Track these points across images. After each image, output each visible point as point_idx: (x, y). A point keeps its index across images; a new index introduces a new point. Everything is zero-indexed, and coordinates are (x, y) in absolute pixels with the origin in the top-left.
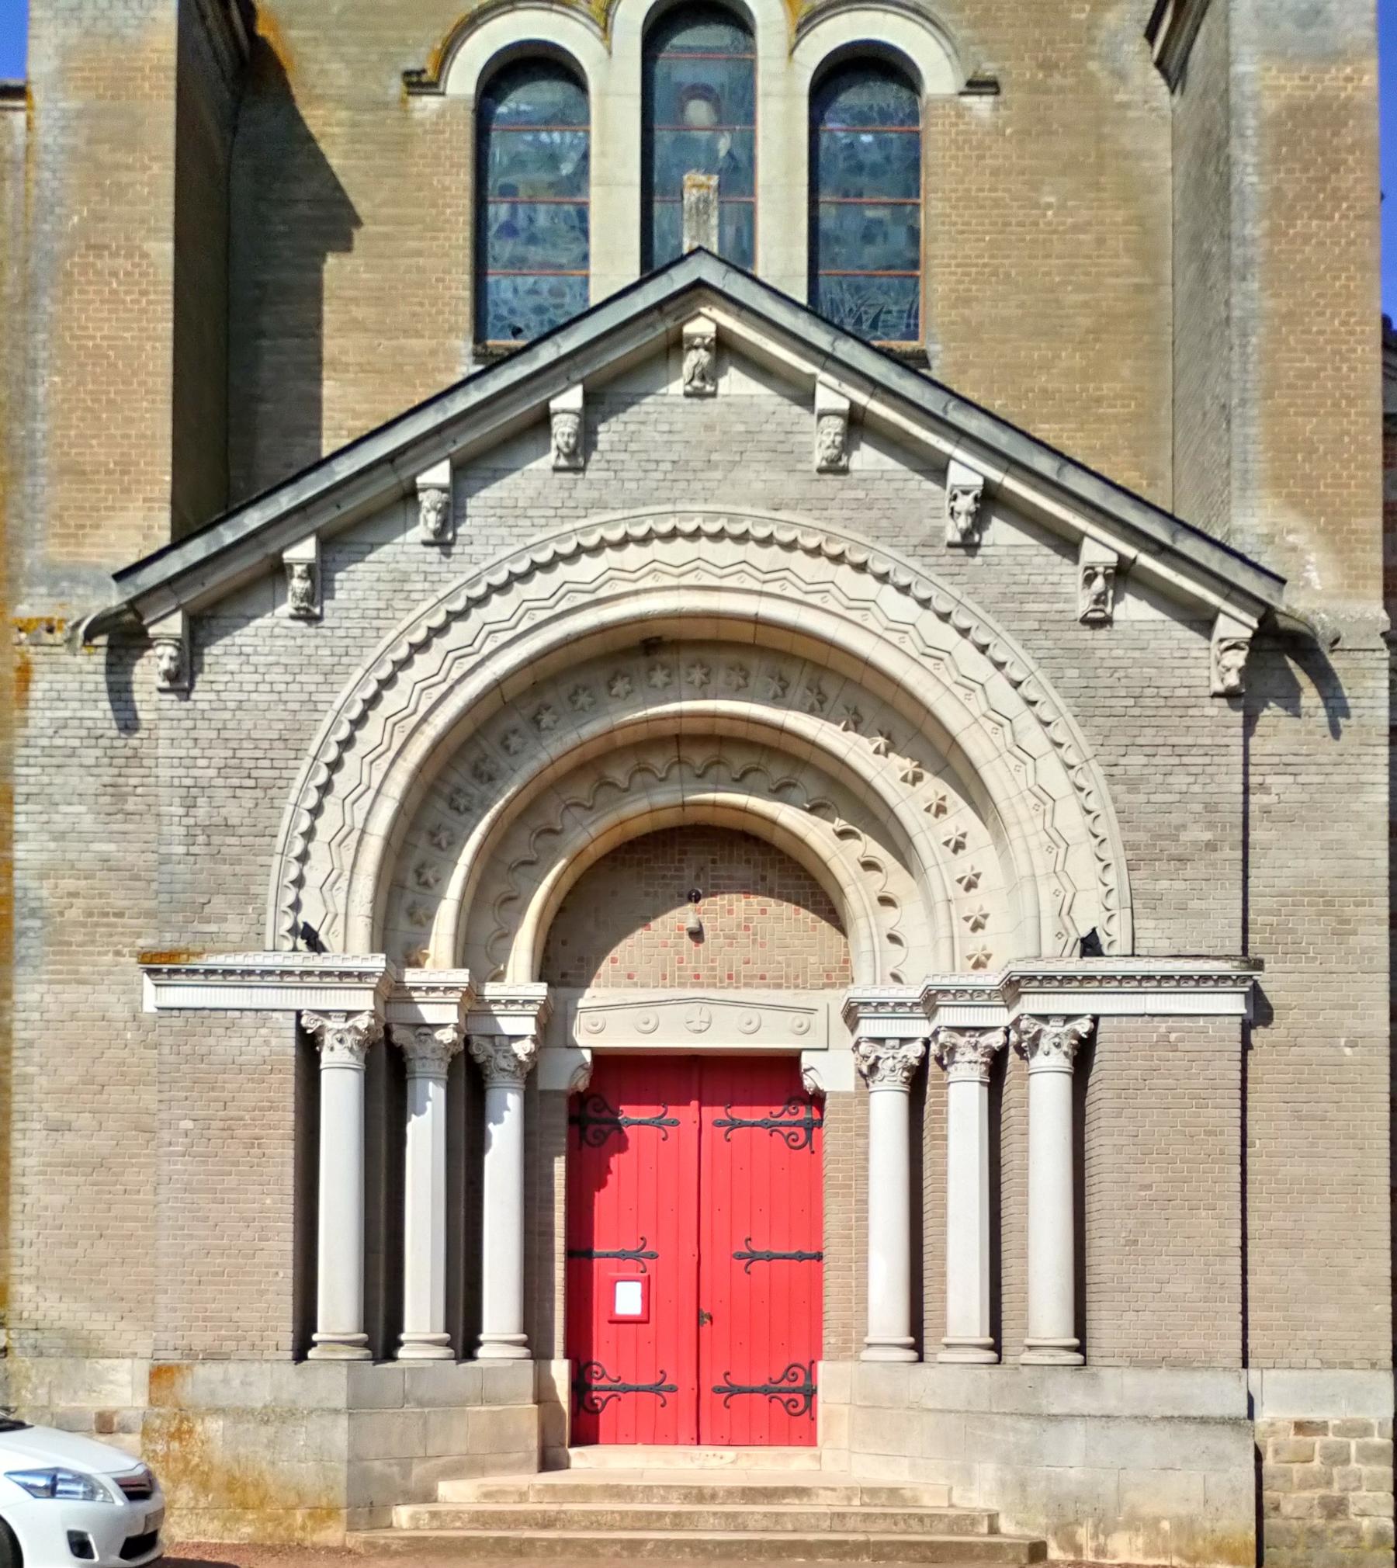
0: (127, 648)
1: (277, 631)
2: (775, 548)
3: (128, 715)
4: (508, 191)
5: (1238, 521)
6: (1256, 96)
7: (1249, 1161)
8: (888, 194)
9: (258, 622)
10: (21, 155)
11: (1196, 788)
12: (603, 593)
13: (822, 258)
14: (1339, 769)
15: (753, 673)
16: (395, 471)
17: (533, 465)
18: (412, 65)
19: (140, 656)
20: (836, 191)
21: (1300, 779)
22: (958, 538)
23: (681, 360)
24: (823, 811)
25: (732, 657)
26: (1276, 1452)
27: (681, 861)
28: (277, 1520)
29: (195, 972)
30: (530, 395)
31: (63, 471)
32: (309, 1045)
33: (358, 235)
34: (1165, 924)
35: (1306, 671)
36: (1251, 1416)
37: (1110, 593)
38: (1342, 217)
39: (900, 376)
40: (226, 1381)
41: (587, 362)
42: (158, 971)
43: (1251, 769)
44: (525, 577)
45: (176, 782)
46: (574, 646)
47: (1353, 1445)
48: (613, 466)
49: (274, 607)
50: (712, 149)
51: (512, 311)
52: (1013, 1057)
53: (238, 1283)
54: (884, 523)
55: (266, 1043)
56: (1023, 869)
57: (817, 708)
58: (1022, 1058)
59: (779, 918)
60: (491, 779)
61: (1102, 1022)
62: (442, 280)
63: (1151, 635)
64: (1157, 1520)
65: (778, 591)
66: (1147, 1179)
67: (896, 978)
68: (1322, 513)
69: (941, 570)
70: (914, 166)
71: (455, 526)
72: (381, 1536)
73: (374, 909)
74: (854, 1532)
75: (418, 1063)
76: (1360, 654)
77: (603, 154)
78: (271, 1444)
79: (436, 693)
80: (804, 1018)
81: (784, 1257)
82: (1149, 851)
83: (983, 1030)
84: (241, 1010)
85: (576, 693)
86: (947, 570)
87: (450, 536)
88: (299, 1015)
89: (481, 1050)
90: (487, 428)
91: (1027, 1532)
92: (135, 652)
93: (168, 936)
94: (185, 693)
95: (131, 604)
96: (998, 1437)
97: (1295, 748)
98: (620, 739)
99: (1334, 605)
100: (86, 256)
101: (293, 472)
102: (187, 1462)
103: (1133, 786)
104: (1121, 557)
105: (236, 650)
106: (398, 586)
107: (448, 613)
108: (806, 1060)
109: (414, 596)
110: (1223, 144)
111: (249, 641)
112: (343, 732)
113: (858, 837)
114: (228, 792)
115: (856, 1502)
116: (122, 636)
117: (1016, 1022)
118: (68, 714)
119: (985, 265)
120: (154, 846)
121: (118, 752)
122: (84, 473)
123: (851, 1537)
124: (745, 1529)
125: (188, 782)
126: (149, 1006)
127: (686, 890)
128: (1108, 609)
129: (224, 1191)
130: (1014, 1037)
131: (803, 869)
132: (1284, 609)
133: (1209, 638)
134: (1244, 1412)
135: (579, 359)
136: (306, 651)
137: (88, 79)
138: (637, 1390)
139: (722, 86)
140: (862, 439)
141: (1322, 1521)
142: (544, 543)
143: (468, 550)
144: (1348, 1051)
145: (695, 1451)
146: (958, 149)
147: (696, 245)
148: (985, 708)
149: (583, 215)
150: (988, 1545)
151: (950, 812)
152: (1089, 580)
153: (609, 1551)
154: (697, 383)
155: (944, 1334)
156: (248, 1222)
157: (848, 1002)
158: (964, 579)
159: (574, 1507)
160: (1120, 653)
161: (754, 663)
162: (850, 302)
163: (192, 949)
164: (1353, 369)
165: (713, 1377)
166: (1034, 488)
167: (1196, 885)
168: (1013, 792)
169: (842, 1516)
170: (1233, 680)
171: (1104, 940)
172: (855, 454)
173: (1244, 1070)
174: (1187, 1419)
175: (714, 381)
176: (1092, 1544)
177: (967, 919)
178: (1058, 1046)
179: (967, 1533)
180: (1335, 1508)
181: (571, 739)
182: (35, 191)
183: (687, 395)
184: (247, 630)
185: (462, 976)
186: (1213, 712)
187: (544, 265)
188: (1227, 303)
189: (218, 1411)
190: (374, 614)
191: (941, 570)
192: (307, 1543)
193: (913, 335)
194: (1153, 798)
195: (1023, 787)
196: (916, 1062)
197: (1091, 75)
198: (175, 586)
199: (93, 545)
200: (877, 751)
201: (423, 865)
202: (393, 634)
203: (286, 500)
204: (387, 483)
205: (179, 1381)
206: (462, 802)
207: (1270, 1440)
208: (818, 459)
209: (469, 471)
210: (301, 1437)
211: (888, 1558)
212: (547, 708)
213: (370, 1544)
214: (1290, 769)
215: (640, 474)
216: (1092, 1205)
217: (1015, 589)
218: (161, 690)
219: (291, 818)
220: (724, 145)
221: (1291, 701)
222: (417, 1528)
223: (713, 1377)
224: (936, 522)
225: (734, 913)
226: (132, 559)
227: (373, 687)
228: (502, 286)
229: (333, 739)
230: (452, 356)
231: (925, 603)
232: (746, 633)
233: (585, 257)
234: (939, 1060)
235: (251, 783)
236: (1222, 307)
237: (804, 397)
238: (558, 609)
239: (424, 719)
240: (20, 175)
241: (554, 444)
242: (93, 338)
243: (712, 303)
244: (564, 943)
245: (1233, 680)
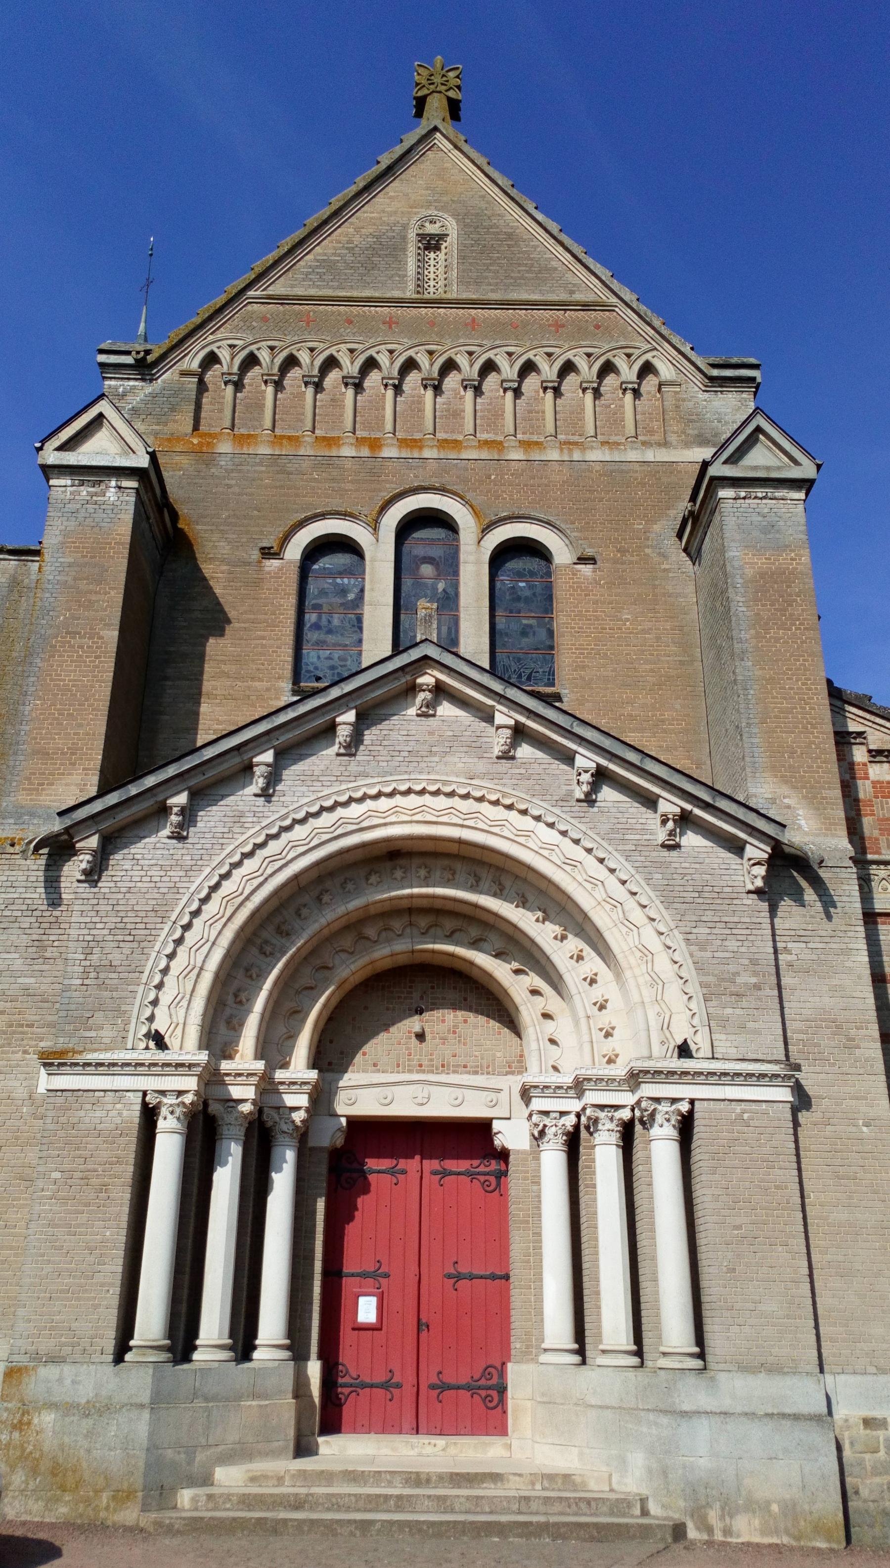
0: (61, 855)
1: (158, 845)
2: (471, 800)
3: (55, 896)
4: (317, 607)
5: (752, 790)
6: (741, 568)
7: (808, 1208)
8: (536, 613)
10: (33, 585)
11: (743, 949)
12: (365, 824)
13: (498, 643)
14: (833, 940)
15: (458, 872)
16: (240, 755)
17: (324, 752)
18: (265, 544)
19: (69, 860)
20: (505, 610)
21: (809, 945)
22: (582, 797)
23: (415, 697)
24: (504, 957)
25: (446, 862)
26: (852, 1444)
27: (411, 987)
28: (87, 1501)
29: (77, 1064)
31: (35, 752)
32: (149, 1116)
33: (228, 629)
34: (733, 1037)
35: (805, 878)
36: (830, 1413)
37: (678, 830)
38: (796, 629)
40: (60, 1380)
41: (359, 697)
42: (52, 1064)
43: (778, 938)
44: (317, 815)
45: (81, 938)
46: (345, 855)
48: (373, 753)
49: (158, 832)
50: (434, 588)
51: (316, 668)
52: (638, 1127)
53: (78, 1299)
54: (537, 787)
55: (120, 1114)
56: (636, 998)
57: (499, 893)
58: (644, 1128)
59: (475, 1027)
60: (288, 934)
61: (697, 1103)
62: (276, 652)
63: (705, 855)
64: (768, 1503)
65: (473, 825)
66: (738, 1221)
67: (555, 1068)
68: (803, 787)
69: (573, 815)
70: (550, 598)
71: (275, 785)
72: (167, 1516)
73: (203, 1020)
74: (537, 1513)
75: (225, 1128)
76: (838, 870)
77: (372, 590)
78: (89, 1435)
79: (256, 883)
80: (493, 1096)
81: (481, 1277)
82: (717, 989)
83: (617, 1107)
84: (105, 1091)
85: (345, 882)
86: (577, 814)
87: (271, 791)
88: (145, 1094)
89: (270, 1117)
90: (290, 735)
91: (671, 1514)
92: (66, 858)
93: (61, 1040)
94: (94, 883)
95: (67, 830)
96: (645, 1430)
97: (804, 926)
98: (372, 910)
99: (818, 840)
100: (66, 637)
101: (178, 754)
102: (23, 1450)
103: (702, 947)
104: (682, 809)
105: (131, 857)
106: (237, 819)
107: (267, 835)
108: (496, 1126)
109: (246, 825)
110: (724, 591)
111: (140, 851)
112: (194, 906)
113: (527, 974)
114: (115, 944)
115: (538, 1486)
116: (59, 849)
117: (639, 1103)
118: (16, 896)
119: (592, 649)
120: (60, 980)
121: (45, 920)
122: (48, 754)
123: (535, 1519)
124: (453, 1511)
126: (41, 1089)
127: (414, 1006)
128: (677, 839)
129: (78, 1226)
130: (637, 1113)
131: (492, 994)
132: (786, 842)
133: (742, 858)
134: (825, 1410)
135: (354, 696)
136: (175, 857)
137: (78, 547)
138: (372, 1386)
139: (440, 557)
140: (523, 741)
142: (328, 796)
143: (282, 799)
144: (865, 1129)
145: (414, 1439)
146: (574, 590)
147: (424, 637)
148: (604, 896)
149: (359, 620)
150: (640, 1526)
151: (586, 960)
152: (664, 822)
153: (345, 1531)
154: (424, 709)
155: (601, 1342)
156: (91, 1250)
157: (523, 1085)
158: (588, 820)
159: (320, 1490)
160: (687, 865)
161: (458, 866)
162: (514, 667)
163: (76, 1048)
164: (811, 708)
165: (429, 1376)
166: (627, 770)
167: (750, 1012)
168: (626, 948)
169: (527, 1499)
170: (759, 883)
171: (693, 1047)
172: (519, 749)
173: (796, 1141)
174: (784, 1416)
175: (434, 708)
177: (601, 1030)
178: (668, 1120)
179: (624, 1515)
181: (341, 910)
182: (39, 604)
183: (418, 715)
185: (260, 1065)
186: (749, 902)
187: (335, 645)
188: (734, 672)
189: (52, 1406)
190: (221, 835)
191: (573, 815)
192: (109, 1523)
193: (553, 685)
194: (716, 955)
195: (632, 945)
196: (571, 1129)
197: (647, 555)
198: (96, 820)
199: (47, 795)
200: (537, 920)
201: (239, 990)
202: (231, 847)
203: (171, 771)
204: (235, 761)
205: (25, 1379)
206: (268, 949)
208: (496, 751)
209: (287, 754)
210: (113, 1429)
211: (564, 1537)
212: (327, 891)
213: (158, 1524)
214: (802, 939)
215: (389, 758)
216: (702, 1240)
217: (620, 826)
218: (79, 881)
219: (155, 960)
220: (441, 586)
221: (798, 897)
222: (196, 1509)
223: (429, 1376)
224: (569, 788)
225: (443, 1021)
226: (72, 803)
227: (216, 879)
228: (310, 655)
229: (187, 910)
230: (279, 692)
231: (564, 833)
232: (454, 848)
233: (360, 641)
234: (587, 1128)
235: (131, 938)
236: (731, 674)
237: (489, 718)
238: (336, 834)
239: (247, 898)
240: (32, 594)
241: (337, 741)
242: (65, 680)
243: (431, 667)
244: (331, 1042)
245: (759, 883)
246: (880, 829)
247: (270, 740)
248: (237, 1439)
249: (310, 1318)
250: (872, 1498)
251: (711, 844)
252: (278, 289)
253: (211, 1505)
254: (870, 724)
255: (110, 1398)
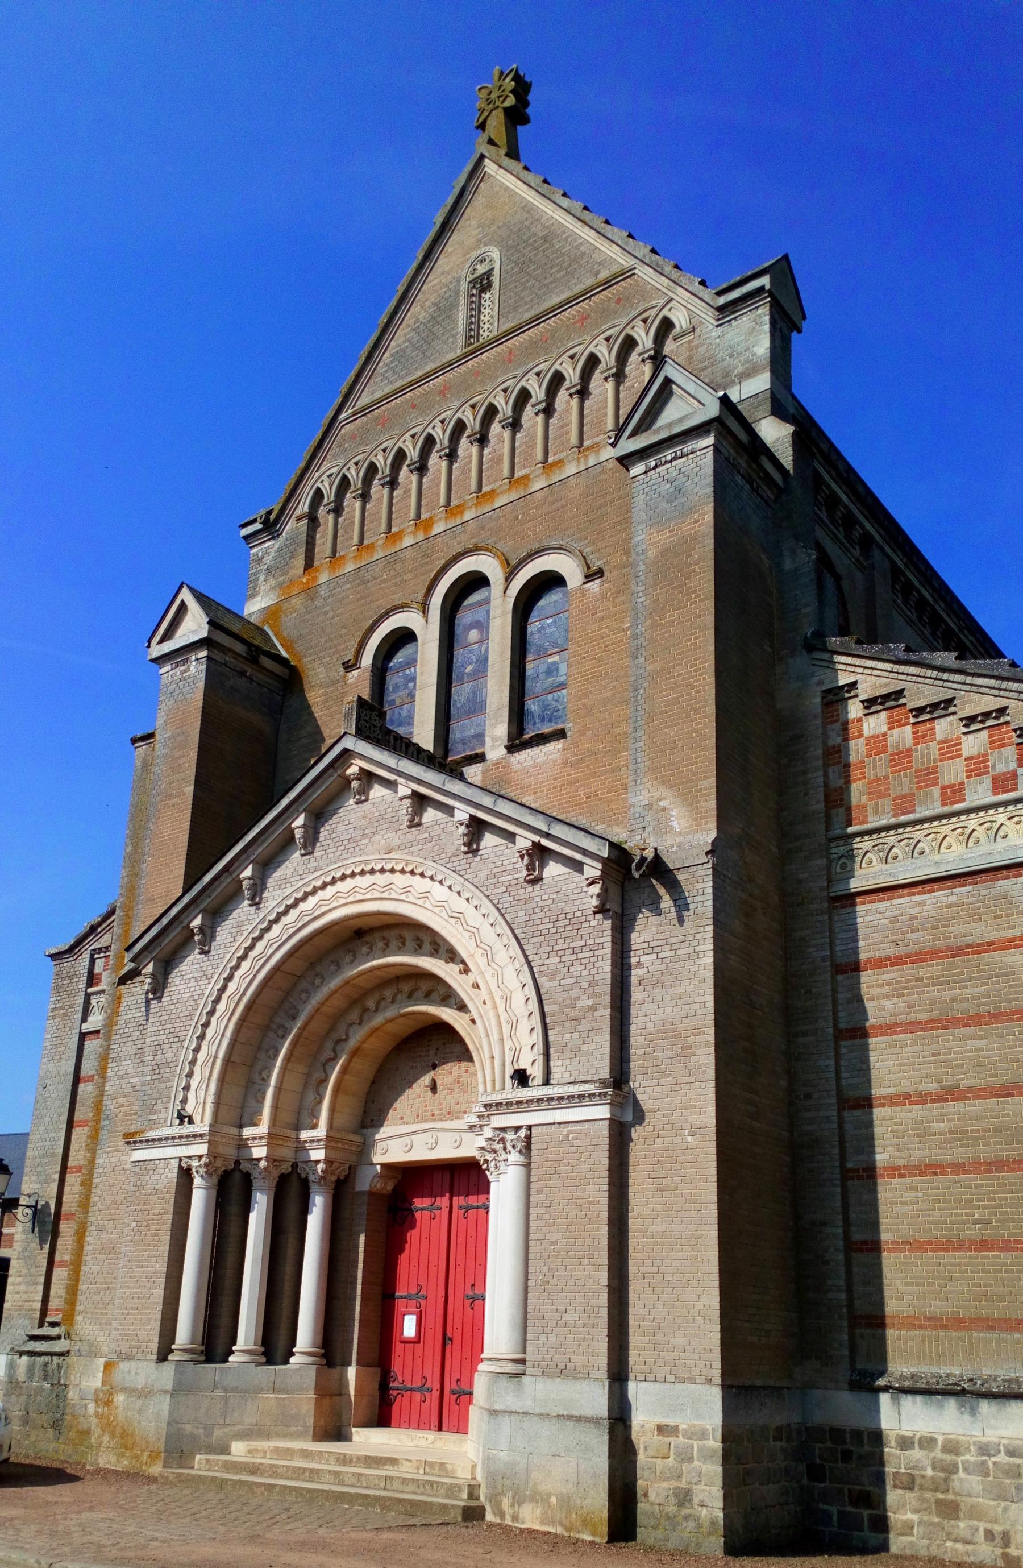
9: (189, 958)
16: (231, 874)
26: (646, 1448)
30: (282, 824)
39: (425, 771)
41: (305, 801)
47: (695, 1445)
64: (549, 1495)
71: (262, 893)
79: (248, 980)
125: (156, 1043)
141: (675, 1508)
144: (689, 1138)
153: (258, 1491)
164: (696, 692)
174: (570, 1417)
176: (511, 1511)
180: (684, 1498)
184: (185, 963)
186: (594, 923)
189: (124, 1390)
207: (642, 1439)
246: (869, 794)
247: (248, 857)
248: (254, 1421)
249: (353, 1333)
250: (658, 1501)
251: (567, 870)
252: (365, 400)
253: (207, 1467)
254: (861, 670)
255: (153, 1385)
